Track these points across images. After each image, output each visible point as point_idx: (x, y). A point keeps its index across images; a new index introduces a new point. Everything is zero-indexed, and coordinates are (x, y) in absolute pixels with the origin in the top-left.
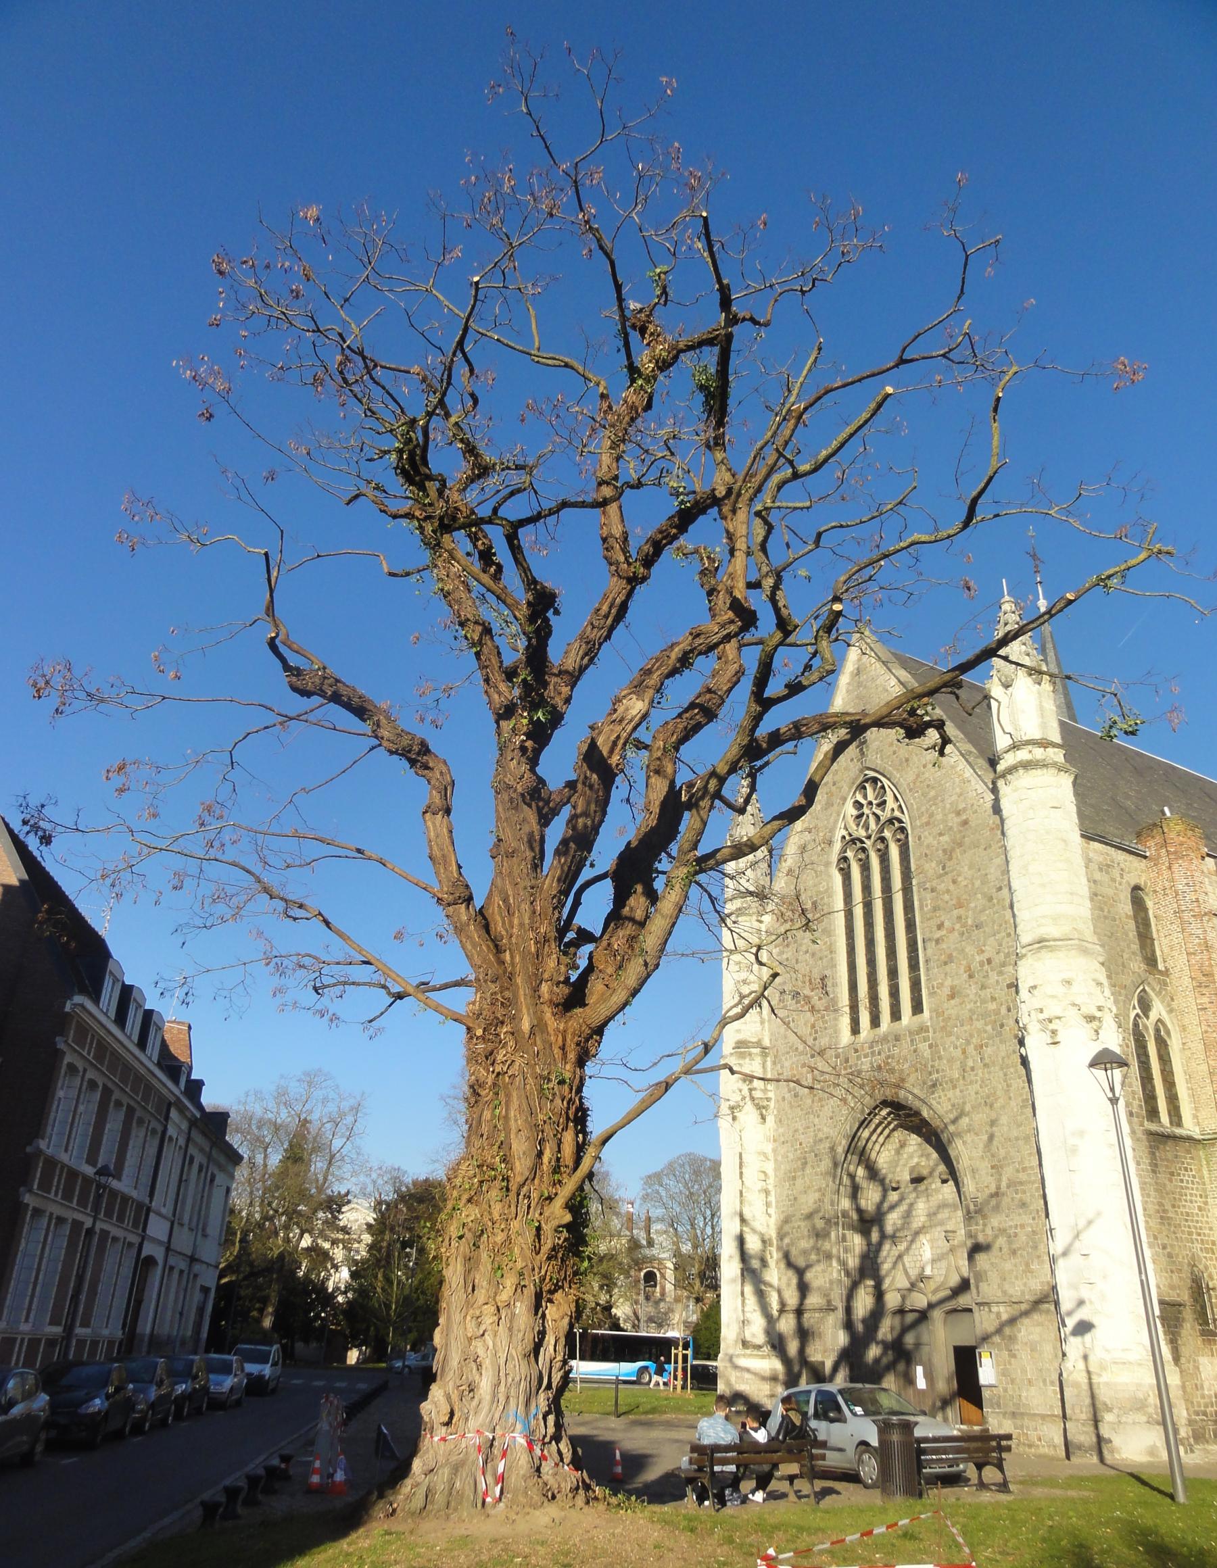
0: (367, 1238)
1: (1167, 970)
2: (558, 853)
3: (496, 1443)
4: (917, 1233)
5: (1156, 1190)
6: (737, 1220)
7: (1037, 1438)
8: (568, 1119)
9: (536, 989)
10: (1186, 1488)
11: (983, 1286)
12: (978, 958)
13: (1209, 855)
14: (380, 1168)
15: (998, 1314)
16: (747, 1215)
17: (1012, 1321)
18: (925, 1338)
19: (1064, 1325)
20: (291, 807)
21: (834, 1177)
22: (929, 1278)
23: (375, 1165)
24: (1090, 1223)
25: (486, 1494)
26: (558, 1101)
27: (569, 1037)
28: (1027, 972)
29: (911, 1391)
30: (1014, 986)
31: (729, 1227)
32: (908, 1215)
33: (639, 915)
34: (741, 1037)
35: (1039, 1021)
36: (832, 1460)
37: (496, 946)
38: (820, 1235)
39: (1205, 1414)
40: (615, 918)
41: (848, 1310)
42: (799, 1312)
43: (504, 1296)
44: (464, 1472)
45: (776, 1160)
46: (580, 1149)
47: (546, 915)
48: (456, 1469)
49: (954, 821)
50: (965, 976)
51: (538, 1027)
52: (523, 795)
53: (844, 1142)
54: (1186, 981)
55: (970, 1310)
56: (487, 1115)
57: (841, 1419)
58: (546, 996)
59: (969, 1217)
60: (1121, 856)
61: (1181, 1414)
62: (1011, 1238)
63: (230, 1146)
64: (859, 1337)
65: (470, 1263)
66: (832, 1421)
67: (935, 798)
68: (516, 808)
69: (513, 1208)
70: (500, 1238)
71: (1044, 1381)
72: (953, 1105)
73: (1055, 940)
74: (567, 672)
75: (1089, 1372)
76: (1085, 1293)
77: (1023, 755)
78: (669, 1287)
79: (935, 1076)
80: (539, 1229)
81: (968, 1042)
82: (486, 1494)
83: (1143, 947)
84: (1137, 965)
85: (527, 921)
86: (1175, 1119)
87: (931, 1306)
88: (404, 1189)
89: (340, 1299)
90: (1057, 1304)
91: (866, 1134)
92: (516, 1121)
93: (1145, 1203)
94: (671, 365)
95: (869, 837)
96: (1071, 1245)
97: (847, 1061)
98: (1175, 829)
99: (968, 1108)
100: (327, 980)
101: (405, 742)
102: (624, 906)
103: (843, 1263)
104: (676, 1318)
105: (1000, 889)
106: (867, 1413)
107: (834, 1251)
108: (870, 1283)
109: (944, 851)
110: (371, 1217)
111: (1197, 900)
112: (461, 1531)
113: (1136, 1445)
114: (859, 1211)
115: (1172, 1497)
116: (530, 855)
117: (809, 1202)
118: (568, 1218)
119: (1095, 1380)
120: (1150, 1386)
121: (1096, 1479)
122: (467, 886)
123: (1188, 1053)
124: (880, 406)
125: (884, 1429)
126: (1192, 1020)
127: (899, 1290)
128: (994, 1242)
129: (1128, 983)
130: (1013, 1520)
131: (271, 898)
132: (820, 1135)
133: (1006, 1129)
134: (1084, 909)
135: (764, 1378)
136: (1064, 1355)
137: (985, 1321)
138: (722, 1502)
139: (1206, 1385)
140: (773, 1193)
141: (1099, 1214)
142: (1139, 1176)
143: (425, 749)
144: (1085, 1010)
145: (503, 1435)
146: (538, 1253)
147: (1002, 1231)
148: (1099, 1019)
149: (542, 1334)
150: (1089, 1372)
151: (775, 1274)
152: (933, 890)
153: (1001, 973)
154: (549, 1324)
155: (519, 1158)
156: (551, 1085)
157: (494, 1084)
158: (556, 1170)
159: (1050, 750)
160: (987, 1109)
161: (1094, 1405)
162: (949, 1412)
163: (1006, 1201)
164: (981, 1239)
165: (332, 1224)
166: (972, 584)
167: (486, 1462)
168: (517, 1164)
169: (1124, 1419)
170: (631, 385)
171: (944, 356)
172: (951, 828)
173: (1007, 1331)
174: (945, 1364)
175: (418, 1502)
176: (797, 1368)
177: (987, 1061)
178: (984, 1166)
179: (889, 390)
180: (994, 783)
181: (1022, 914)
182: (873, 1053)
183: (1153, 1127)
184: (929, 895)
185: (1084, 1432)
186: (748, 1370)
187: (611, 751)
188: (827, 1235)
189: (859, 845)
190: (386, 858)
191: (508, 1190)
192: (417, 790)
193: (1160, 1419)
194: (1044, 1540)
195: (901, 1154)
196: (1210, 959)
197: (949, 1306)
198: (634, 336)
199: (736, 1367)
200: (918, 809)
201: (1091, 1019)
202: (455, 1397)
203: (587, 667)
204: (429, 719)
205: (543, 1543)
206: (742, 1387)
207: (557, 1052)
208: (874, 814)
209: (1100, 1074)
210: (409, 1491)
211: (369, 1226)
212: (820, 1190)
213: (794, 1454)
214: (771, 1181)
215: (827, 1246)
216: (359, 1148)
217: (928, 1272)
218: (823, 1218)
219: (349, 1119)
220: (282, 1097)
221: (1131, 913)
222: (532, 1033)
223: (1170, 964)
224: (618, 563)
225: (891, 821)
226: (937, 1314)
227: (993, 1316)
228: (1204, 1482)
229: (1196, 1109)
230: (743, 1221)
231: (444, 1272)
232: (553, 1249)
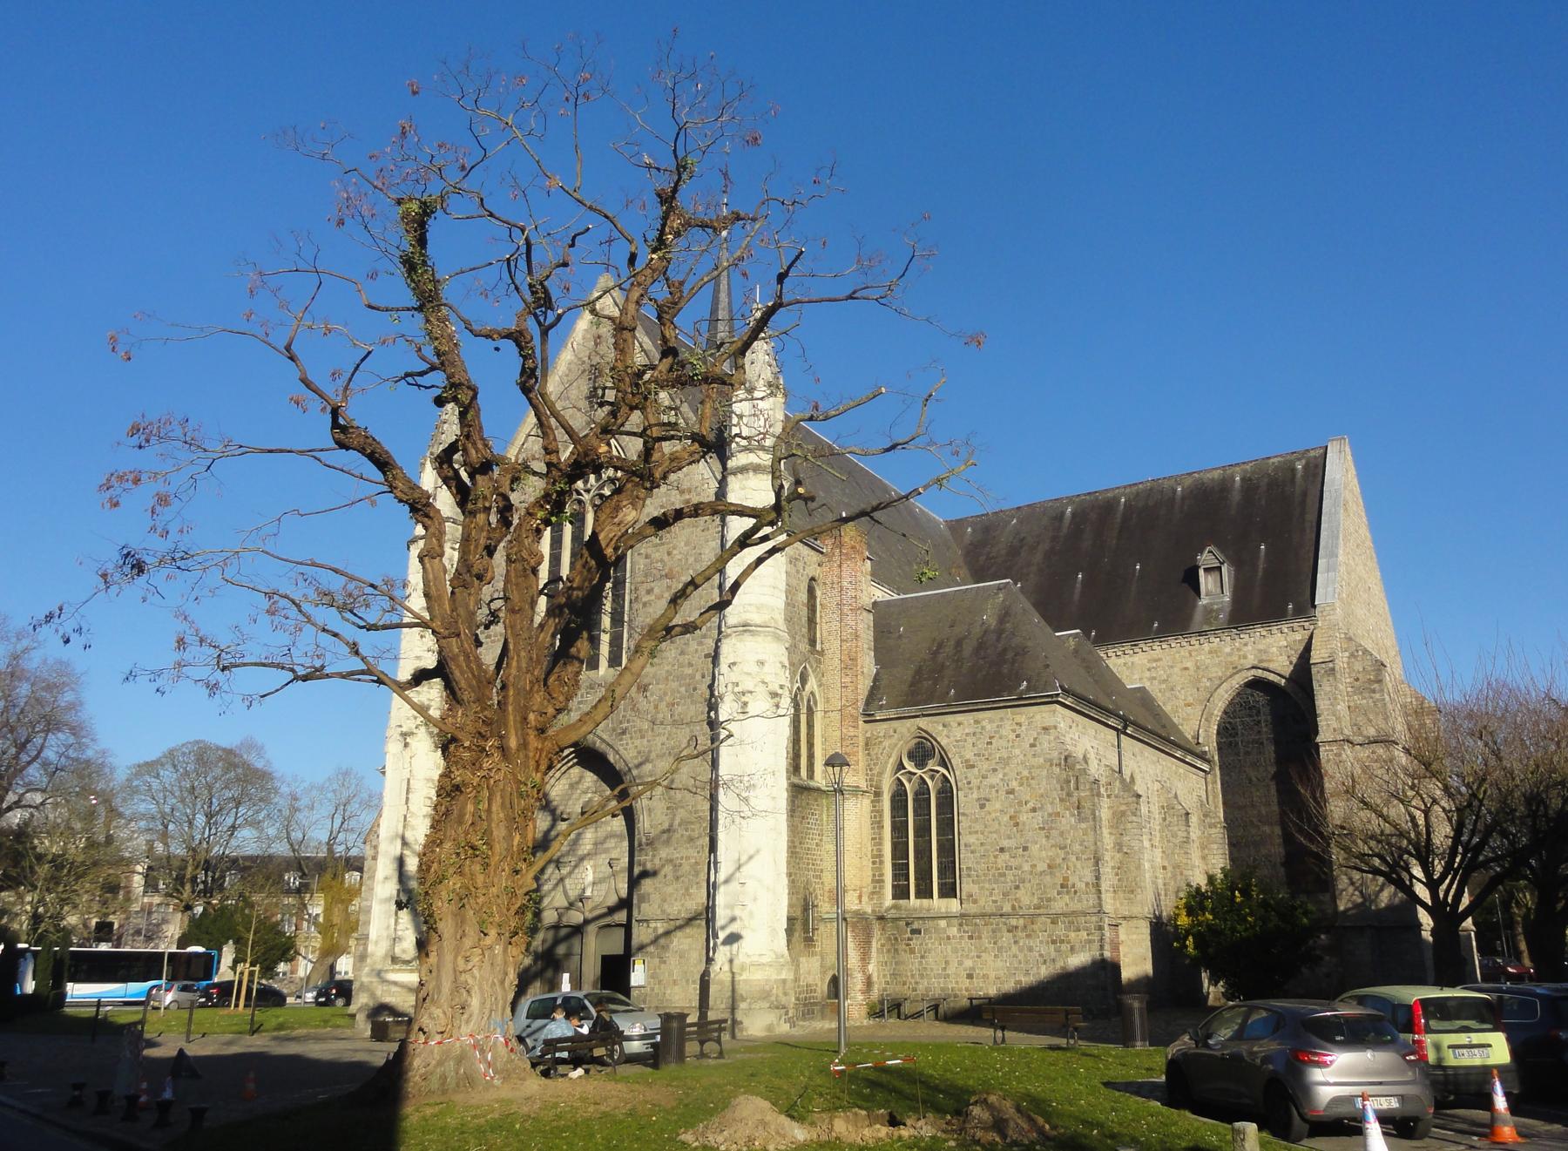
4: (582, 859)
6: (399, 843)
17: (667, 933)
18: (577, 949)
24: (751, 858)
32: (576, 842)
51: (524, 745)
56: (470, 808)
62: (677, 867)
76: (737, 912)
84: (804, 646)
87: (587, 922)
95: (588, 491)
99: (653, 755)
119: (737, 978)
126: (835, 694)
141: (758, 851)
144: (771, 688)
153: (700, 643)
163: (677, 836)
164: (649, 866)
173: (662, 941)
183: (795, 780)
186: (395, 983)
197: (603, 922)
201: (774, 695)
206: (387, 1000)
207: (532, 763)
226: (592, 929)
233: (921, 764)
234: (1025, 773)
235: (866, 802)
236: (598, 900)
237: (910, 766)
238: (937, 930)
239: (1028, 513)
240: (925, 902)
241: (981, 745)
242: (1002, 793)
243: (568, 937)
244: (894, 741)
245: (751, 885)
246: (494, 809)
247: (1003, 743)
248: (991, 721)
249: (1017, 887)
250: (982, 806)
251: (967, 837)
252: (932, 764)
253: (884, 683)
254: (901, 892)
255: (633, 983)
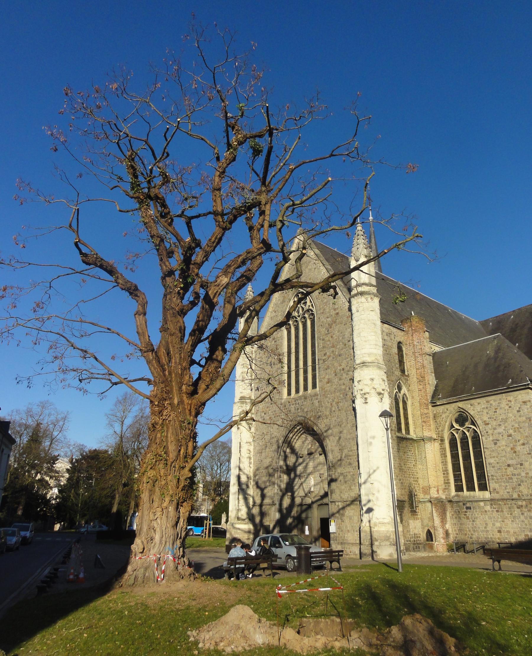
0: (67, 475)
1: (408, 375)
2: (191, 335)
3: (161, 559)
4: (309, 474)
5: (399, 459)
7: (352, 552)
8: (191, 437)
9: (180, 388)
10: (402, 567)
11: (334, 495)
12: (339, 368)
13: (427, 331)
14: (74, 445)
15: (338, 506)
16: (242, 466)
17: (343, 508)
18: (310, 515)
19: (362, 510)
20: (77, 307)
21: (278, 452)
22: (312, 492)
23: (73, 443)
24: (374, 471)
25: (158, 577)
26: (187, 431)
27: (192, 406)
28: (358, 375)
29: (303, 536)
30: (352, 380)
31: (234, 472)
32: (306, 467)
33: (219, 358)
34: (242, 395)
35: (361, 394)
36: (279, 562)
37: (163, 369)
38: (271, 475)
39: (410, 541)
40: (209, 359)
41: (281, 505)
42: (261, 506)
43: (165, 504)
44: (149, 570)
45: (254, 445)
46: (195, 448)
47: (185, 359)
48: (146, 569)
49: (333, 313)
50: (334, 374)
51: (181, 402)
52: (178, 312)
53: (282, 439)
54: (415, 379)
55: (328, 504)
56: (159, 435)
57: (281, 547)
58: (185, 390)
59: (329, 469)
60: (394, 330)
61: (402, 541)
63: (10, 436)
64: (284, 514)
65: (152, 492)
66: (277, 547)
67: (326, 303)
68: (175, 317)
69: (169, 471)
70: (163, 482)
71: (354, 531)
72: (326, 425)
73: (369, 363)
74: (197, 263)
75: (370, 527)
76: (371, 497)
77: (360, 289)
78: (200, 495)
79: (319, 414)
80: (179, 479)
81: (333, 401)
82: (158, 577)
83: (400, 365)
84: (398, 373)
85: (178, 361)
86: (407, 432)
87: (313, 503)
88: (85, 454)
89: (54, 502)
90: (360, 501)
91: (291, 435)
92: (171, 438)
93: (394, 463)
94: (243, 143)
95: (299, 316)
96: (367, 479)
97: (285, 406)
98: (415, 320)
100: (84, 377)
101: (129, 285)
102: (214, 354)
103: (279, 486)
104: (203, 508)
105: (349, 341)
106: (291, 544)
107: (276, 482)
108: (290, 494)
109: (329, 324)
110: (69, 466)
111: (421, 349)
112: (150, 591)
113: (385, 553)
114: (287, 466)
115: (397, 570)
116: (179, 335)
117: (267, 462)
118: (190, 475)
119: (373, 529)
120: (392, 531)
121: (371, 566)
122: (152, 345)
123: (414, 407)
124: (326, 184)
125: (299, 549)
126: (416, 394)
127: (300, 497)
128: (338, 478)
129: (394, 379)
130: (345, 579)
131: (74, 348)
132: (273, 436)
133: (345, 435)
134: (379, 351)
135: (245, 532)
136: (362, 521)
137: (333, 508)
138: (238, 578)
139: (411, 530)
140: (252, 458)
141: (378, 468)
142: (393, 453)
143: (136, 289)
144: (378, 390)
145: (164, 556)
146: (178, 488)
147: (342, 474)
148: (383, 394)
149: (179, 518)
150: (370, 527)
151: (252, 491)
152: (323, 340)
153: (347, 374)
154: (181, 514)
155: (172, 452)
156: (185, 424)
157: (162, 424)
158: (185, 457)
159: (372, 288)
160: (339, 427)
161: (371, 539)
162: (317, 543)
163: (344, 462)
164: (334, 477)
165: (51, 469)
166: (350, 233)
167: (157, 566)
168: (171, 454)
169: (381, 544)
170: (227, 151)
171: (347, 155)
172: (332, 315)
173: (341, 512)
174: (316, 524)
175: (131, 581)
176: (259, 528)
177: (340, 408)
178: (336, 449)
179: (330, 179)
180: (350, 299)
181: (357, 352)
182: (296, 404)
184: (321, 342)
185: (367, 549)
186: (239, 529)
187: (214, 297)
188: (274, 475)
189: (295, 319)
190: (120, 332)
191: (167, 464)
192: (133, 305)
193: (395, 543)
194: (356, 585)
195: (303, 443)
196: (424, 371)
197: (319, 503)
198: (230, 129)
199: (234, 528)
200: (319, 306)
201: (379, 394)
202: (145, 543)
203: (205, 261)
204: (129, 268)
205: (183, 593)
207: (187, 411)
208: (301, 307)
209: (383, 419)
210: (128, 576)
211: (68, 470)
212: (272, 457)
213: (265, 560)
214: (252, 453)
215: (273, 480)
216: (65, 436)
217: (312, 490)
218: (272, 468)
219: (61, 423)
220: (29, 413)
221: (397, 352)
222: (178, 404)
223: (410, 372)
224: (219, 222)
225: (308, 310)
226: (315, 506)
227: (336, 506)
228: (409, 565)
229: (415, 428)
230: (240, 469)
231: (141, 496)
232: (184, 487)
233: (462, 425)
234: (516, 425)
235: (437, 445)
236: (316, 492)
237: (456, 426)
238: (479, 507)
239: (519, 313)
240: (472, 493)
241: (491, 413)
242: (505, 437)
243: (306, 510)
244: (447, 414)
245: (376, 484)
246: (169, 435)
247: (502, 411)
248: (495, 401)
249: (520, 485)
250: (495, 444)
251: (490, 459)
252: (467, 424)
253: (440, 388)
254: (459, 488)
255: (331, 531)
